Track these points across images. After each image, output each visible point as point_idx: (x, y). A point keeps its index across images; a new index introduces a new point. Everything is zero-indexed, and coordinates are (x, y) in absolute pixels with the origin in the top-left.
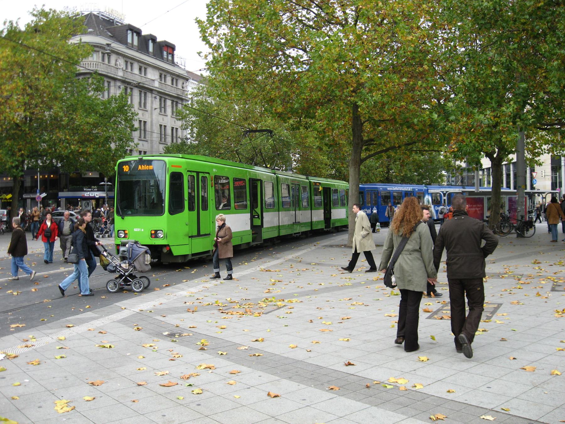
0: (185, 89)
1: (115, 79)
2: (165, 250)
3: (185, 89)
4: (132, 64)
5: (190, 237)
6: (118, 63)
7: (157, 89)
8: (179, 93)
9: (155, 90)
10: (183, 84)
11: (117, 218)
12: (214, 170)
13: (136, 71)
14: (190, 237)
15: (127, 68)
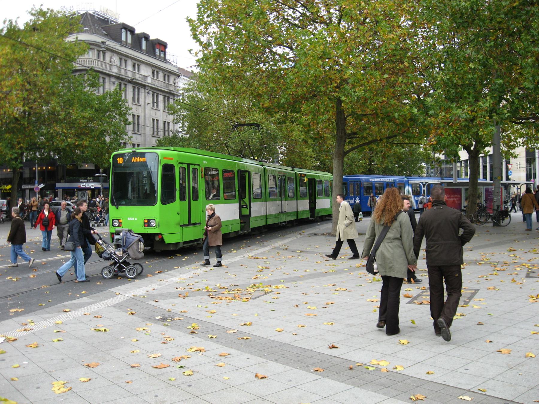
0: (176, 85)
1: (109, 76)
2: (157, 238)
3: (176, 85)
4: (126, 61)
5: (181, 226)
6: (112, 60)
7: (150, 85)
8: (171, 88)
9: (148, 86)
10: (175, 80)
11: (112, 208)
12: (204, 162)
13: (130, 68)
14: (181, 226)
15: (121, 64)
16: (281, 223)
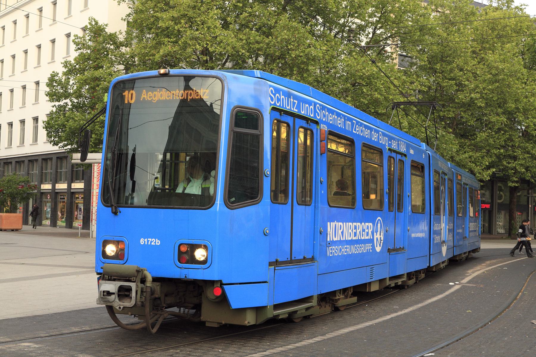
5: (271, 264)
14: (271, 264)
16: (277, 307)
